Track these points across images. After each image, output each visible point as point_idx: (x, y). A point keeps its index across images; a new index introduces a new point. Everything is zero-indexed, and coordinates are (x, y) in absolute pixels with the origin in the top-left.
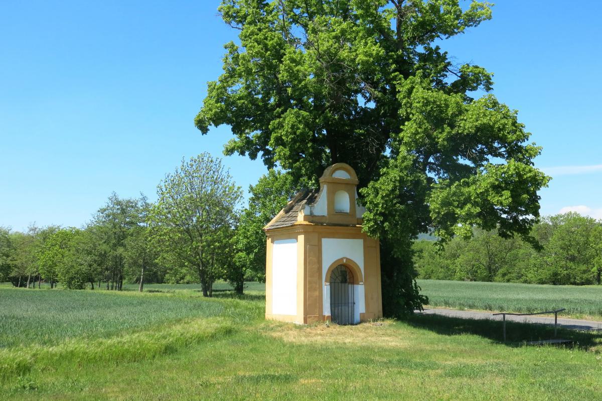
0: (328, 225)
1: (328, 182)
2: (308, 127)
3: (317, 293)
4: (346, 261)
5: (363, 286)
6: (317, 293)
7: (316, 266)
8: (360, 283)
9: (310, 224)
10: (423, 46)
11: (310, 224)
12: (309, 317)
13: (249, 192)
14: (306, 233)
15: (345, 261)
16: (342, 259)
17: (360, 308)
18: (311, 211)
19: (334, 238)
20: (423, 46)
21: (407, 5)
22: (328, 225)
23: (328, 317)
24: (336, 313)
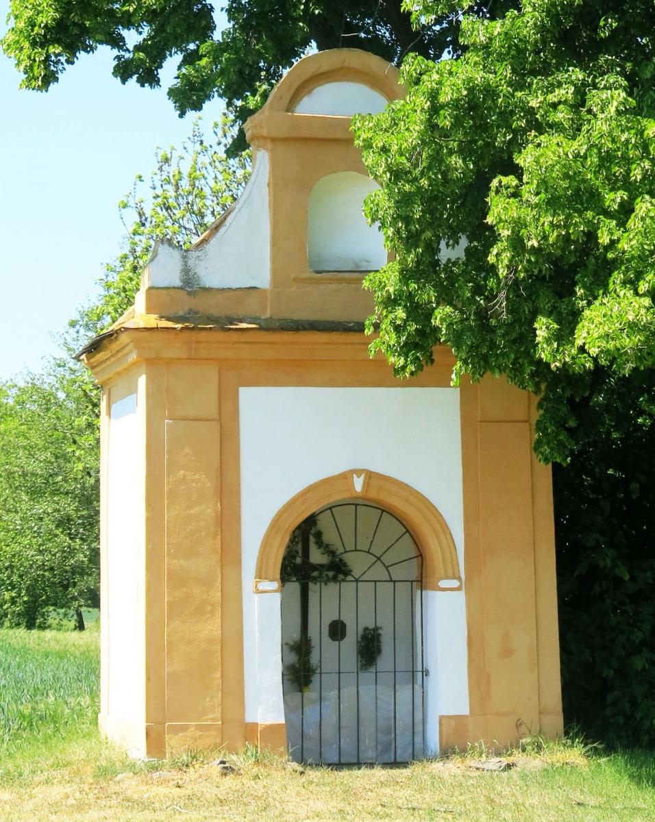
0: (267, 327)
1: (273, 140)
2: (69, 17)
3: (211, 627)
4: (367, 485)
5: (460, 597)
6: (211, 627)
7: (209, 510)
8: (443, 584)
9: (170, 324)
10: (128, 253)
11: (170, 324)
12: (175, 730)
13: (114, 59)
14: (152, 363)
15: (358, 484)
16: (346, 477)
17: (448, 690)
18: (186, 270)
19: (302, 383)
20: (128, 253)
21: (641, 283)
22: (267, 327)
23: (271, 729)
24: (311, 731)
